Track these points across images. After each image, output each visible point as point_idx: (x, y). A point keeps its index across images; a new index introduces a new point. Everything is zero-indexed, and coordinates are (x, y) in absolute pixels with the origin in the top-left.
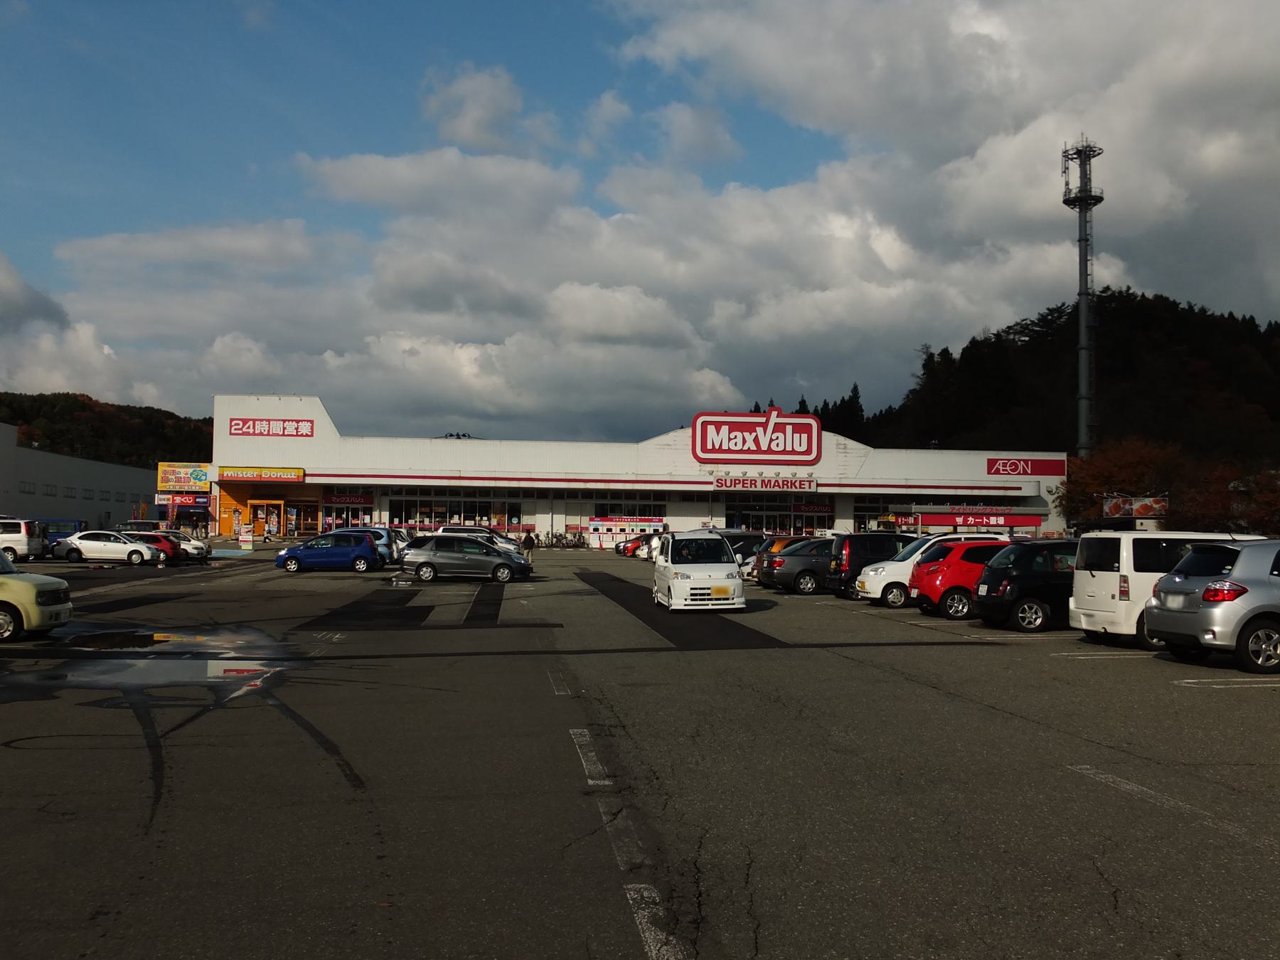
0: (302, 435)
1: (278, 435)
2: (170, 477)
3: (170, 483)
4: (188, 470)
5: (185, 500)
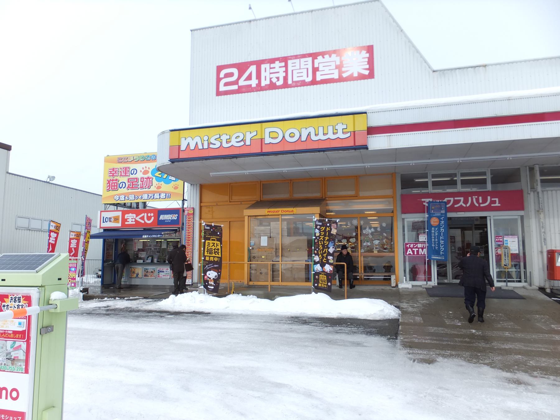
0: (350, 78)
1: (303, 84)
3: (121, 191)
5: (142, 218)
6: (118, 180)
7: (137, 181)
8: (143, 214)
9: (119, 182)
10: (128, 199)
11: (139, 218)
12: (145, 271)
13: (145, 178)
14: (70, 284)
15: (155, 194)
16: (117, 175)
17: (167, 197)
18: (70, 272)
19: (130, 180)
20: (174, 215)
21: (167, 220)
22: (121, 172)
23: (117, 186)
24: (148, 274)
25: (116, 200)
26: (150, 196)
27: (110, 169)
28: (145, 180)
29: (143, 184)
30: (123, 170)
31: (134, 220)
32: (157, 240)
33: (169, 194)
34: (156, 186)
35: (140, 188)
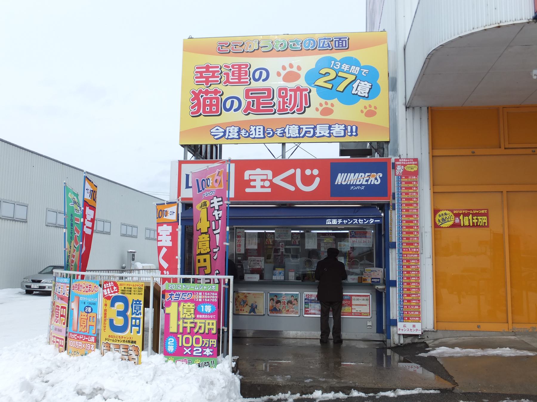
2: (229, 91)
3: (227, 117)
4: (296, 61)
5: (291, 180)
6: (220, 92)
7: (269, 96)
8: (292, 171)
9: (224, 98)
10: (248, 136)
11: (282, 180)
12: (273, 299)
13: (291, 90)
14: (200, 349)
15: (318, 126)
16: (217, 81)
17: (349, 134)
18: (198, 316)
19: (251, 94)
20: (373, 174)
21: (356, 185)
22: (227, 74)
23: (217, 105)
24: (280, 306)
25: (216, 137)
26: (304, 130)
27: (197, 68)
28: (289, 93)
29: (284, 103)
30: (233, 70)
31: (267, 184)
32: (292, 231)
33: (354, 128)
34: (320, 109)
35: (278, 111)
